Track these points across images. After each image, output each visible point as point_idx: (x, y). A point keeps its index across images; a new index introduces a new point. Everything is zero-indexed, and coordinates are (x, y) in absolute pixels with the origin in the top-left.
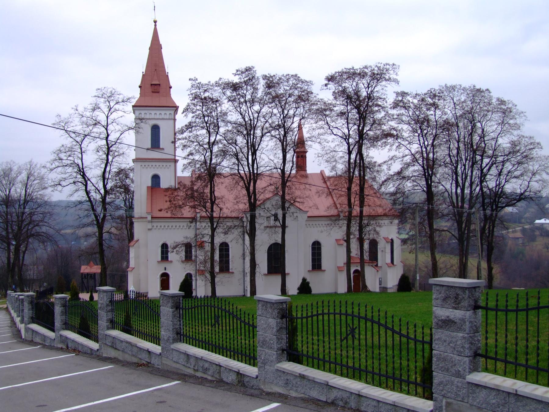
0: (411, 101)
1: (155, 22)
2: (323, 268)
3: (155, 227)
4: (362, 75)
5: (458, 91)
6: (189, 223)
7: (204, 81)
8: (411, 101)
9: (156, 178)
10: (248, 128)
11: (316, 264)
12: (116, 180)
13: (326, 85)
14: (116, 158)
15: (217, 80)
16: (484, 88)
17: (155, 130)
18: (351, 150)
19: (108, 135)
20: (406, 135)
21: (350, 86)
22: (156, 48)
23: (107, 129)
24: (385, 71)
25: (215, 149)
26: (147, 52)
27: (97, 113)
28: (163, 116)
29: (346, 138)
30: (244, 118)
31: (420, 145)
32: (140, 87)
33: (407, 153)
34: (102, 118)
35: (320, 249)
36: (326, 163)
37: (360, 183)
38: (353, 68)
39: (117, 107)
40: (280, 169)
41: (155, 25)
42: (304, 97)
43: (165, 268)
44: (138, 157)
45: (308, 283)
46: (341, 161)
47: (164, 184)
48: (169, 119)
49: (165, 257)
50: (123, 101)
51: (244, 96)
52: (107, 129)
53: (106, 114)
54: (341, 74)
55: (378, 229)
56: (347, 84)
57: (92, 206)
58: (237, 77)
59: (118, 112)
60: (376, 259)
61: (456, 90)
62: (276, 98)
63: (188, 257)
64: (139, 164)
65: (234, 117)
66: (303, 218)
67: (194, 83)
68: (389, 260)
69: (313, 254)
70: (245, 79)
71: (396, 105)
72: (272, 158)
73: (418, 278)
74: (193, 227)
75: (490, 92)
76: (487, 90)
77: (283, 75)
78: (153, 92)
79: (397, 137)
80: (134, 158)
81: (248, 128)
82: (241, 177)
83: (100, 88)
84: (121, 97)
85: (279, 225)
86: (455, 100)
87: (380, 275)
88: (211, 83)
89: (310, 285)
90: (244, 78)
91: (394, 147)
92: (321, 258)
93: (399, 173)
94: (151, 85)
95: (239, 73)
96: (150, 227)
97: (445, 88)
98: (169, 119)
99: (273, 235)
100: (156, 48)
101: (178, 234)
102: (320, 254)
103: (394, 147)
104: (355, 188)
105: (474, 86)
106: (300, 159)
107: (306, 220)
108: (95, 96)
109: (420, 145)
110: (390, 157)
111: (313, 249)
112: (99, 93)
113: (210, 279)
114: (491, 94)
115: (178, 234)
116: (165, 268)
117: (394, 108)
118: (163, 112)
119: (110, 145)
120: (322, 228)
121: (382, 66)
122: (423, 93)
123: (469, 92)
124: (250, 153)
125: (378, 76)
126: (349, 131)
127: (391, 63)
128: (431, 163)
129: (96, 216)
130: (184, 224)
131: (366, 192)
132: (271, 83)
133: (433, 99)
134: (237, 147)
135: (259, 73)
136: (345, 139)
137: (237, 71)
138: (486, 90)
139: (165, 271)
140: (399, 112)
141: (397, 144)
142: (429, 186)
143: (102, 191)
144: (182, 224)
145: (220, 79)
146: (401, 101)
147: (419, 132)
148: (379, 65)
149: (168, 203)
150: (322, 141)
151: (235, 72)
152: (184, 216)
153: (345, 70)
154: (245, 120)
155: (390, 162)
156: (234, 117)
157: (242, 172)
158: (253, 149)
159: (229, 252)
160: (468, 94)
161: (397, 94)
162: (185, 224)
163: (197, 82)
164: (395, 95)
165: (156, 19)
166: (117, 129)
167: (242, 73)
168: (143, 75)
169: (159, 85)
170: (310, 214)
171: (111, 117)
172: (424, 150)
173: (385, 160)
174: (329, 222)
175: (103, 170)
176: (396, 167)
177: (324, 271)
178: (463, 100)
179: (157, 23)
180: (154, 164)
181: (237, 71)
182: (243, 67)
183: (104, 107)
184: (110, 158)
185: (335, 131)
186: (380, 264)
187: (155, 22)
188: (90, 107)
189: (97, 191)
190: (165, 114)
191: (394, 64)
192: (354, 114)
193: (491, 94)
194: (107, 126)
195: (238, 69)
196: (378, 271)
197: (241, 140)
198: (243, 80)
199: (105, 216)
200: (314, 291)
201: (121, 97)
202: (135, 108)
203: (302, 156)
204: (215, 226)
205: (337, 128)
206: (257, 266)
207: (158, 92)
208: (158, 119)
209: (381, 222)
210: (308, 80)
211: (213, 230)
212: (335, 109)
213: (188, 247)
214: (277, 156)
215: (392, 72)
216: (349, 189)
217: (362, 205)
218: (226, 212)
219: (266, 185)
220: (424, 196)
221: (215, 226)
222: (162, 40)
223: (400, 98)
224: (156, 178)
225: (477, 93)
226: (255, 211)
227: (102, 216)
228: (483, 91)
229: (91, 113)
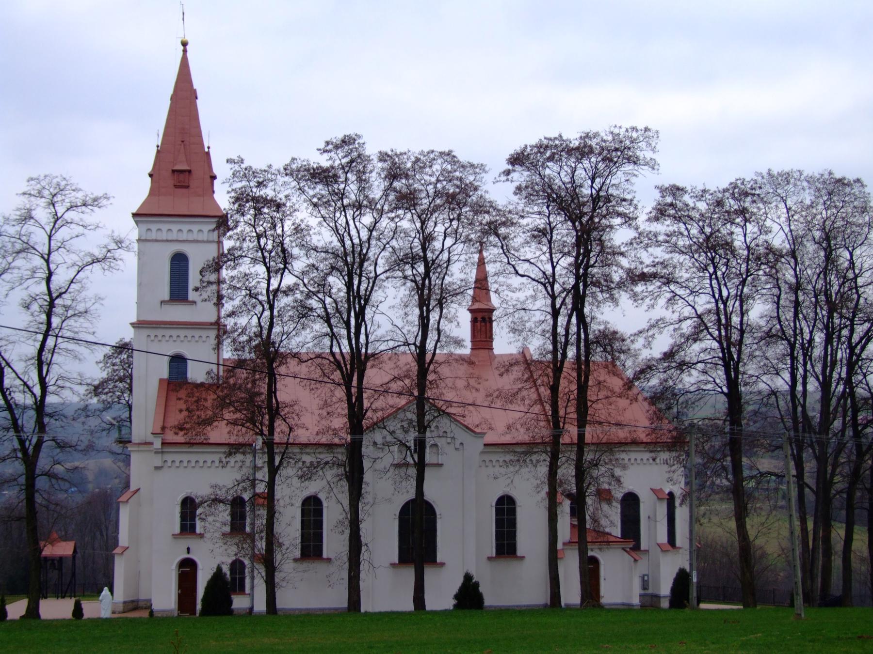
0: (692, 205)
1: (185, 44)
2: (519, 553)
3: (169, 464)
4: (582, 151)
5: (795, 185)
6: (223, 456)
7: (258, 164)
8: (692, 205)
9: (178, 362)
10: (351, 262)
11: (506, 546)
12: (114, 365)
13: (508, 173)
14: (71, 322)
15: (288, 161)
16: (851, 176)
17: (179, 262)
18: (558, 306)
19: (50, 274)
20: (683, 275)
21: (557, 173)
22: (184, 96)
23: (47, 261)
24: (628, 143)
25: (283, 301)
26: (168, 103)
27: (29, 227)
28: (195, 236)
29: (549, 281)
30: (342, 241)
31: (714, 296)
32: (151, 175)
33: (686, 314)
34: (39, 238)
35: (513, 512)
36: (511, 335)
37: (579, 376)
38: (560, 136)
39: (69, 216)
40: (414, 344)
41: (185, 51)
42: (458, 197)
43: (188, 549)
44: (141, 319)
45: (477, 585)
46: (539, 330)
47: (196, 373)
48: (208, 242)
49: (188, 526)
50: (85, 205)
51: (342, 195)
52: (47, 261)
53: (48, 229)
54: (541, 148)
55: (618, 472)
56: (550, 170)
57: (15, 420)
58: (326, 156)
59: (73, 226)
60: (637, 538)
61: (792, 181)
62: (407, 200)
63: (237, 524)
64: (145, 332)
65: (323, 237)
66: (475, 446)
67: (237, 167)
68: (662, 536)
69: (499, 523)
70: (344, 161)
71: (660, 213)
72: (400, 325)
73: (695, 580)
74: (248, 464)
75: (863, 186)
76: (858, 181)
77: (422, 153)
78: (176, 186)
79: (669, 281)
80: (134, 320)
81: (351, 262)
82: (337, 364)
83: (35, 176)
84: (80, 195)
85: (412, 462)
86: (789, 203)
87: (642, 567)
88: (274, 168)
89: (481, 589)
90: (338, 159)
91: (662, 301)
92: (515, 532)
93: (669, 356)
94: (173, 171)
95: (330, 147)
96: (159, 464)
97: (766, 176)
98: (208, 242)
99: (404, 483)
100: (184, 96)
101: (212, 475)
102: (513, 523)
103: (662, 301)
104: (568, 385)
105: (830, 173)
106: (478, 324)
107: (482, 452)
108: (24, 194)
109: (714, 296)
110: (653, 322)
111: (499, 511)
112: (34, 188)
113: (264, 574)
114: (867, 190)
115: (212, 475)
116: (188, 549)
117: (657, 219)
118: (195, 228)
119: (54, 295)
120: (497, 468)
121: (622, 132)
122: (721, 189)
123: (819, 185)
124: (353, 314)
125: (617, 153)
126: (554, 268)
127: (641, 126)
128: (735, 336)
129: (22, 442)
130: (214, 456)
131: (591, 395)
132: (395, 171)
133: (740, 201)
134: (328, 300)
135: (371, 150)
136: (544, 285)
137: (328, 143)
138: (855, 181)
139: (187, 556)
140: (671, 229)
141: (669, 295)
142: (733, 383)
143: (37, 390)
144: (209, 458)
145: (293, 159)
146: (671, 205)
147: (711, 270)
148: (616, 131)
149: (185, 413)
150: (500, 289)
151: (322, 146)
152: (210, 441)
153: (545, 142)
154: (344, 246)
155: (650, 333)
156: (323, 237)
157: (336, 350)
158: (358, 303)
159: (322, 516)
160: (819, 190)
161: (663, 190)
162: (216, 458)
163: (243, 166)
164: (657, 195)
165: (188, 38)
166: (70, 262)
167: (337, 147)
168: (158, 152)
169: (190, 171)
170: (490, 438)
171: (60, 235)
172: (721, 306)
173: (640, 328)
174: (508, 457)
175: (38, 345)
176: (662, 343)
177: (442, 564)
178: (808, 202)
179: (188, 47)
180: (175, 333)
181: (328, 143)
182: (338, 135)
183: (42, 214)
184: (56, 321)
185: (522, 268)
186: (644, 546)
187: (185, 44)
188: (16, 214)
189: (27, 390)
190: (200, 231)
191: (647, 129)
192: (564, 233)
193: (867, 190)
194: (49, 254)
195: (328, 139)
196: (635, 560)
197: (337, 283)
198: (337, 163)
199: (40, 443)
200: (488, 601)
201: (80, 195)
202: (139, 219)
203: (483, 319)
204: (277, 463)
205: (528, 261)
206: (364, 549)
207: (187, 187)
208: (184, 241)
209: (623, 456)
210: (475, 163)
211: (273, 471)
212: (523, 222)
213: (237, 505)
214: (410, 318)
215: (643, 145)
216: (554, 389)
217: (582, 422)
218: (302, 435)
219: (386, 380)
220: (722, 403)
221: (277, 463)
222: (198, 82)
223: (669, 200)
224: (178, 362)
225: (835, 187)
226: (585, 427)
227: (34, 440)
228: (849, 184)
229: (18, 228)
